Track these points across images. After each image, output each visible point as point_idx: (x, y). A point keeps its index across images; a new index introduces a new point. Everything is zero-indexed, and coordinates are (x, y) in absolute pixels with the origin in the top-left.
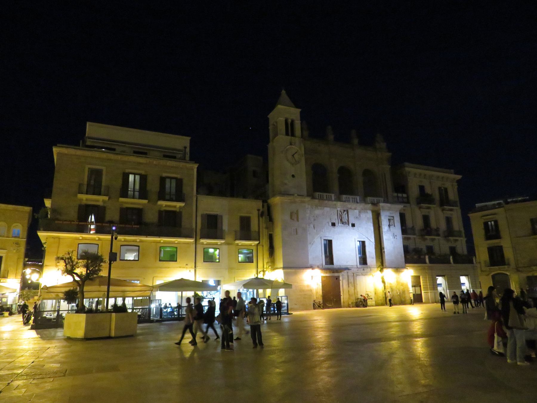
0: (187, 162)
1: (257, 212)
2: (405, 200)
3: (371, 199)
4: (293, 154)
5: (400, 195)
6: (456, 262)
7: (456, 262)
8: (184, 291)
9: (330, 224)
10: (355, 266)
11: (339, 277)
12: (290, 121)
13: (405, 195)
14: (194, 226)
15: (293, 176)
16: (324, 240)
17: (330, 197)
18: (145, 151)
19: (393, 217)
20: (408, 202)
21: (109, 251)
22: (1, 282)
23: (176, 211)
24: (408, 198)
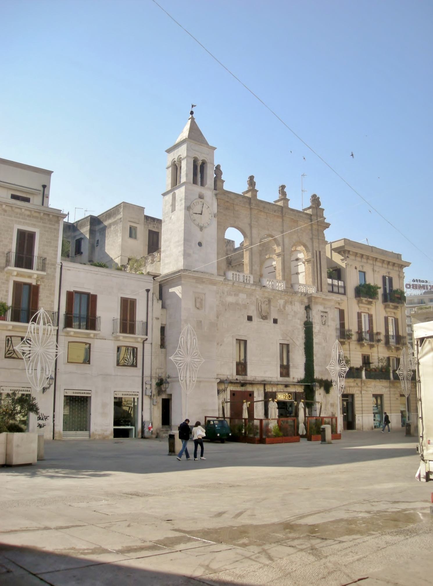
0: (5, 203)
1: (146, 293)
2: (342, 290)
3: (235, 274)
4: (200, 215)
5: (336, 282)
6: (368, 376)
7: (368, 376)
8: (254, 417)
10: (274, 378)
11: (253, 392)
12: (200, 163)
13: (341, 283)
14: (56, 310)
15: (200, 244)
16: (237, 339)
17: (238, 276)
18: (28, 196)
19: (326, 312)
20: (345, 294)
21: (421, 383)
22: (138, 404)
23: (90, 293)
24: (344, 287)
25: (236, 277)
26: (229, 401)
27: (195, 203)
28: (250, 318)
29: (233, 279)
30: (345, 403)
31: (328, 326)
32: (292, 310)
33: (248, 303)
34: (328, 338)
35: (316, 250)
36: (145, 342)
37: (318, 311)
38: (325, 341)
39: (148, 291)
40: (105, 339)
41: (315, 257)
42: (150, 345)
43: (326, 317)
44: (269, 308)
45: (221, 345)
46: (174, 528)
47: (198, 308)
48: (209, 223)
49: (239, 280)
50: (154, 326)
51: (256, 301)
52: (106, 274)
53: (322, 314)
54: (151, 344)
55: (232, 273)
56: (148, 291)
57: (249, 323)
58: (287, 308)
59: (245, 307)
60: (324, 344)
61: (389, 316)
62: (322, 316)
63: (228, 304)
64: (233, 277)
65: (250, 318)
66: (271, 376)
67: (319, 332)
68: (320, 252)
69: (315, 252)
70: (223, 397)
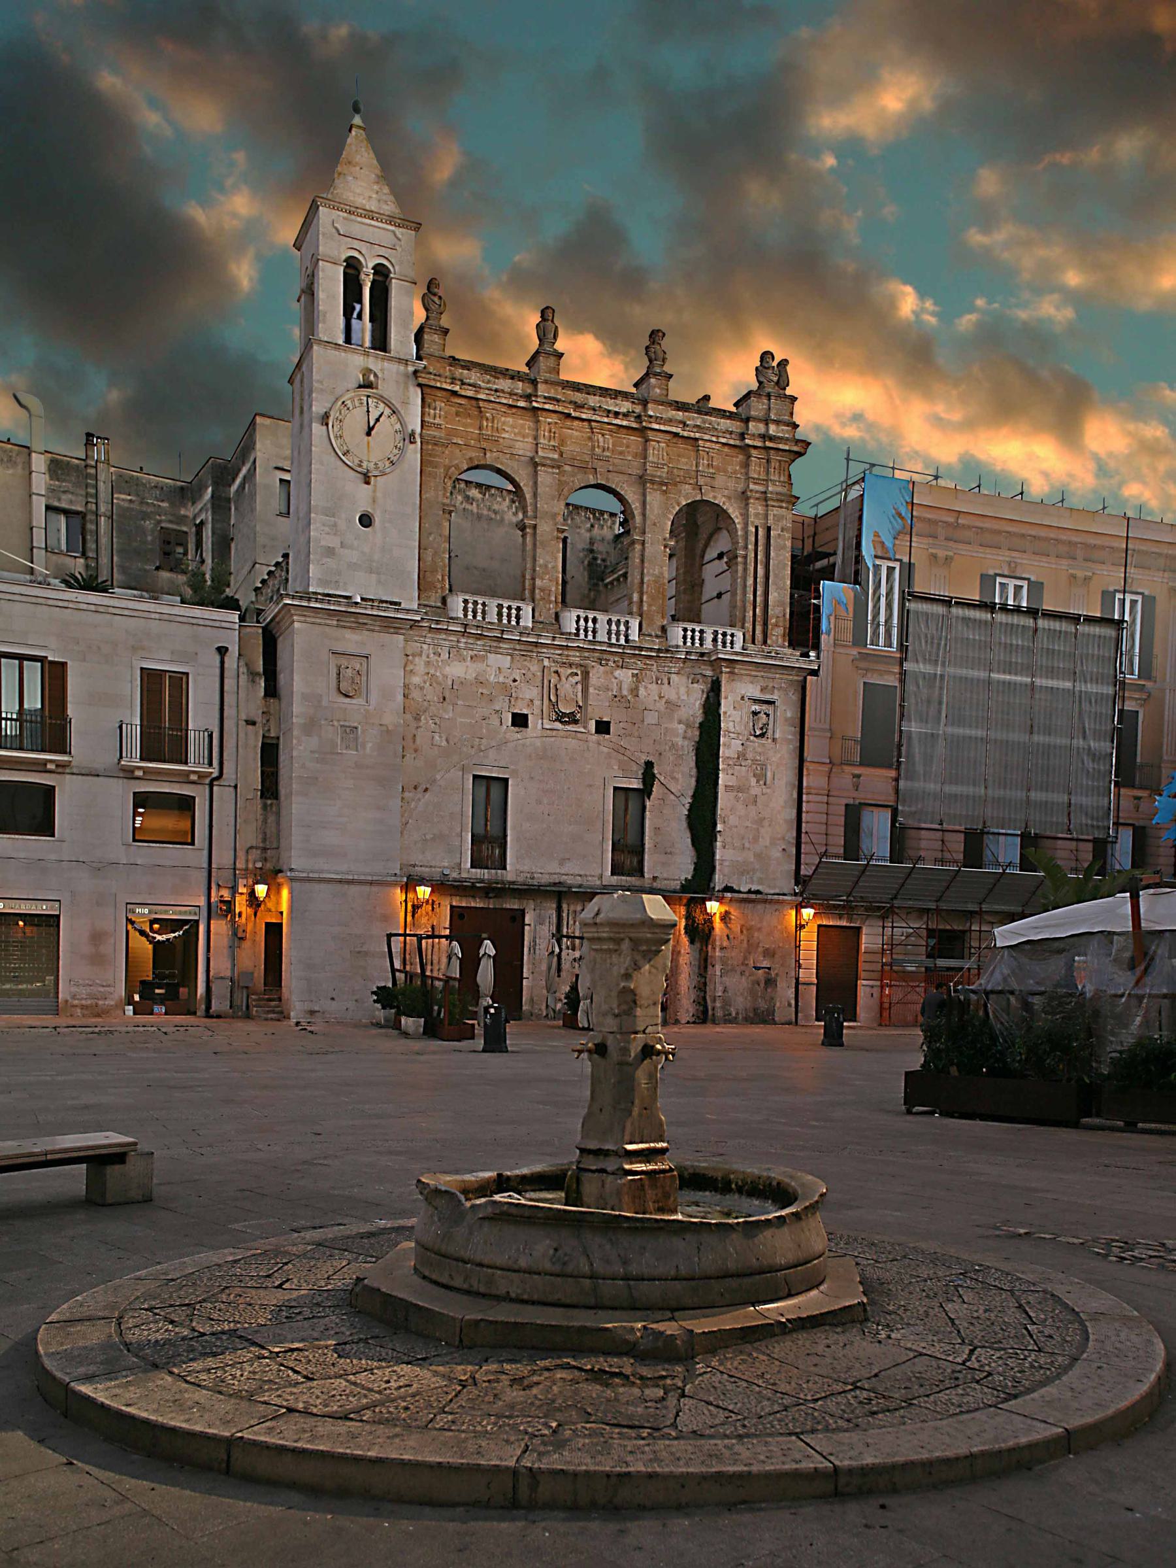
9: (509, 719)
17: (514, 612)
25: (693, 638)
26: (447, 932)
27: (349, 403)
28: (520, 721)
29: (466, 615)
30: (186, 1467)
31: (774, 740)
32: (660, 697)
33: (515, 681)
34: (769, 774)
35: (757, 522)
36: (215, 783)
37: (742, 698)
38: (762, 782)
39: (222, 651)
40: (98, 776)
41: (751, 547)
42: (232, 789)
43: (768, 715)
44: (585, 691)
45: (426, 790)
46: (776, 907)
47: (347, 696)
48: (395, 459)
49: (518, 623)
50: (240, 743)
51: (539, 674)
52: (93, 608)
53: (756, 707)
54: (236, 787)
55: (461, 600)
56: (222, 651)
57: (514, 734)
58: (642, 692)
59: (508, 691)
60: (756, 790)
61: (134, 823)
62: (755, 713)
63: (450, 683)
64: (465, 610)
65: (520, 721)
66: (582, 873)
67: (741, 756)
68: (769, 529)
69: (754, 530)
70: (430, 922)
